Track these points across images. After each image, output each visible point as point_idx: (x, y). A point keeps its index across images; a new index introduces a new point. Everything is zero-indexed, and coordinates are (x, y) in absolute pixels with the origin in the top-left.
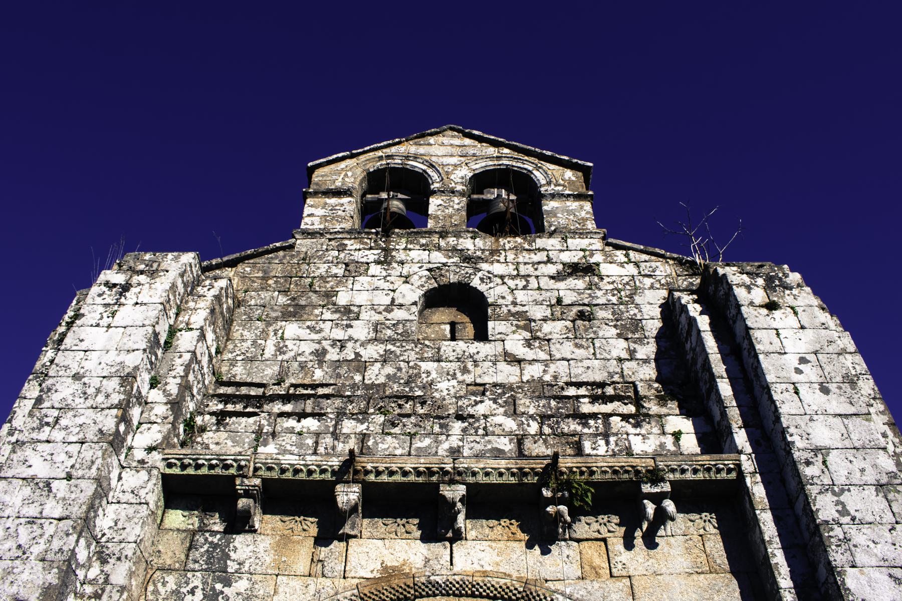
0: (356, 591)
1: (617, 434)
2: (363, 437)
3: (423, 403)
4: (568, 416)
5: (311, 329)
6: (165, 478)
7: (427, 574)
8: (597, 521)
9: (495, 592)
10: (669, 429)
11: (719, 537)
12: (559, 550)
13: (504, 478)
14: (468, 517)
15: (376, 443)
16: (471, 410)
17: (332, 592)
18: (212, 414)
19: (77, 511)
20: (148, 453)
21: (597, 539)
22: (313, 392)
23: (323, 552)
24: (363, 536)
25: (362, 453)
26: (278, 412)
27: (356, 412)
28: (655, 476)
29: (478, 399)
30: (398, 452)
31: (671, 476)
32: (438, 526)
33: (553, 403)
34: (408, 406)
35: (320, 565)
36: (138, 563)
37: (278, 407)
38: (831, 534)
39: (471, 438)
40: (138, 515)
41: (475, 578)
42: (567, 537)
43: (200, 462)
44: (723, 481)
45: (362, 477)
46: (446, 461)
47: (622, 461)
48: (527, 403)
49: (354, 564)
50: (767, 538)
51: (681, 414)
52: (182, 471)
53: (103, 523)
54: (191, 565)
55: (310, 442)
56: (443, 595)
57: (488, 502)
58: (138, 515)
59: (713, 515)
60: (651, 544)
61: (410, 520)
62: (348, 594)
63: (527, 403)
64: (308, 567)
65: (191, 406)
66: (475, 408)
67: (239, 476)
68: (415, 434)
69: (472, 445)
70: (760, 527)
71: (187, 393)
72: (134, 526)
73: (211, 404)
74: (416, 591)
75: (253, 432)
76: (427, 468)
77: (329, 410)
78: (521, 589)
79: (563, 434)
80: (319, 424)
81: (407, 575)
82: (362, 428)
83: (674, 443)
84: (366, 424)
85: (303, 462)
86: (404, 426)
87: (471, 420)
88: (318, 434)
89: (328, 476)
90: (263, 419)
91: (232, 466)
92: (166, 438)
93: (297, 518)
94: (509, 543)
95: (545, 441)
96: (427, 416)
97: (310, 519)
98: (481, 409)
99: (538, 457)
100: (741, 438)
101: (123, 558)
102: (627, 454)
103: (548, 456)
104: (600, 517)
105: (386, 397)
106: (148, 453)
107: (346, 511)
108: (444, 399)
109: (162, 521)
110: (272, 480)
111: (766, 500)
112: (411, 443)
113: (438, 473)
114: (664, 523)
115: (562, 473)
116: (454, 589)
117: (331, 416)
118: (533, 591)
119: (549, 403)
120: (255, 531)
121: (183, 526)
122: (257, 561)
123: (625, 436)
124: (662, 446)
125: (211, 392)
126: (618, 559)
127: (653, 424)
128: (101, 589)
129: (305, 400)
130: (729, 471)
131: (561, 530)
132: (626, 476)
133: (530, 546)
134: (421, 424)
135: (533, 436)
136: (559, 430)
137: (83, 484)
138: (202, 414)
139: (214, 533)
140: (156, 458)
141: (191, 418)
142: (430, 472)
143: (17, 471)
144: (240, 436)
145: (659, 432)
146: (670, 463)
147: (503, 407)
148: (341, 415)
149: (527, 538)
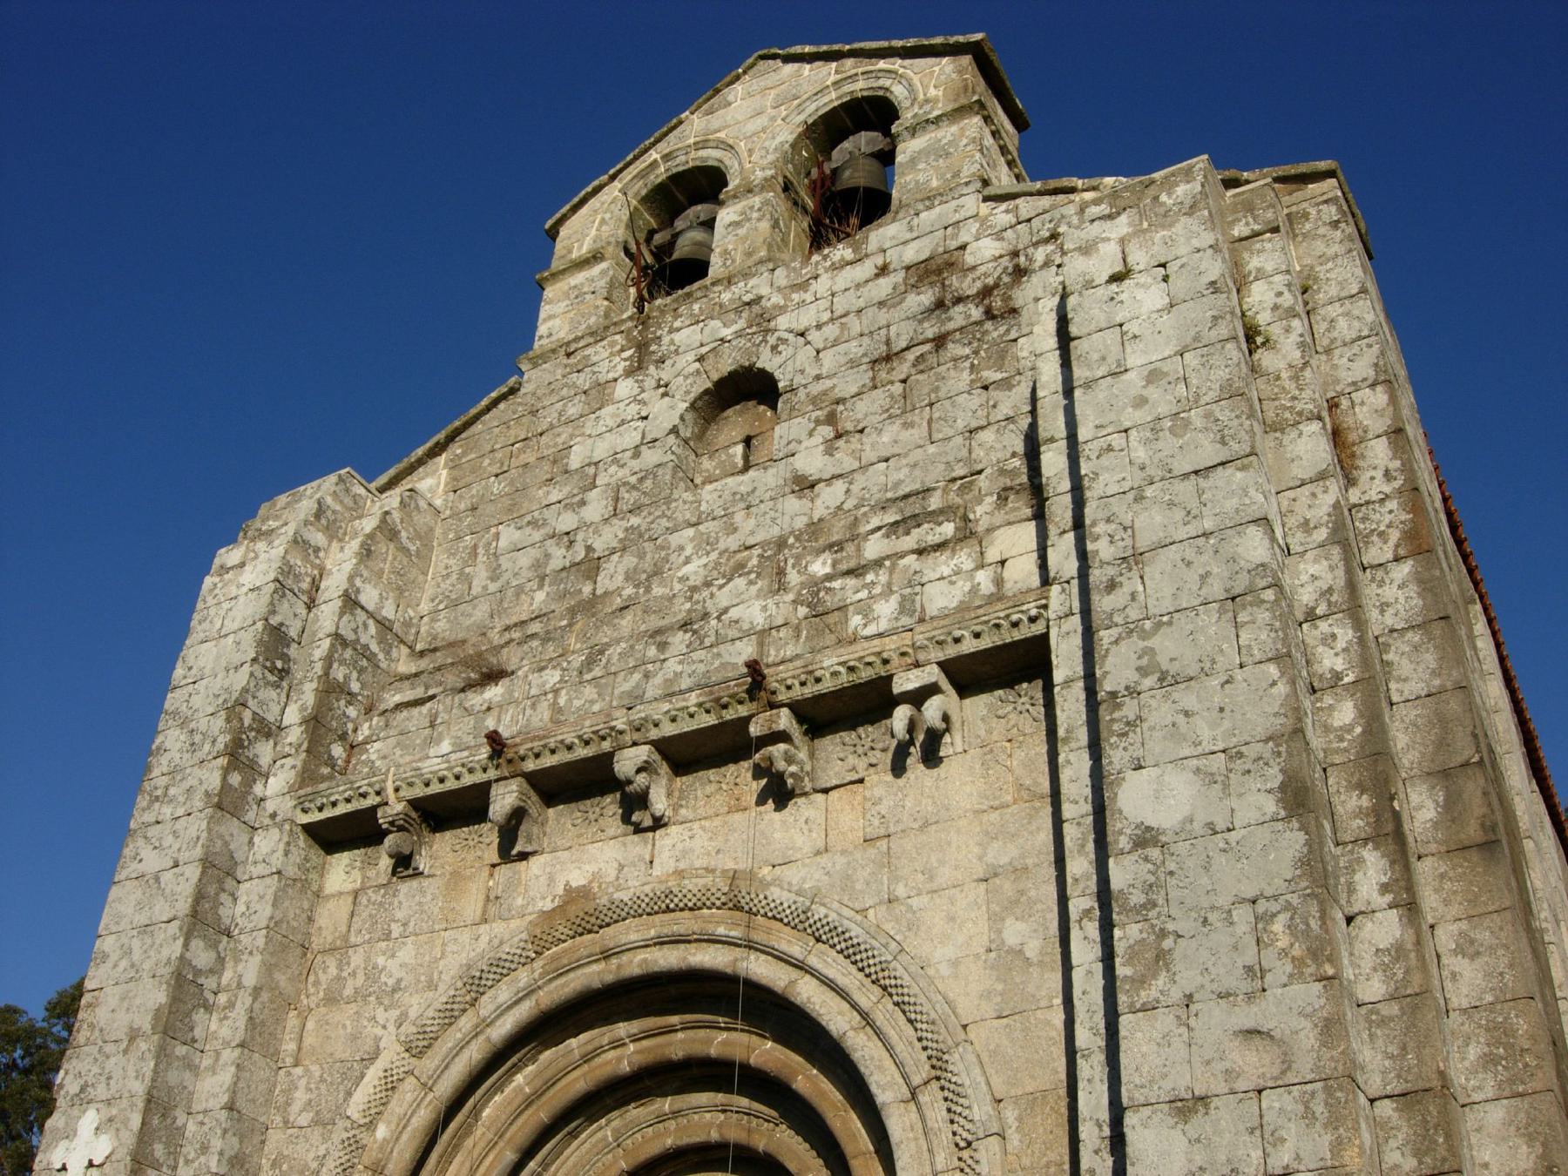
5: (533, 524)
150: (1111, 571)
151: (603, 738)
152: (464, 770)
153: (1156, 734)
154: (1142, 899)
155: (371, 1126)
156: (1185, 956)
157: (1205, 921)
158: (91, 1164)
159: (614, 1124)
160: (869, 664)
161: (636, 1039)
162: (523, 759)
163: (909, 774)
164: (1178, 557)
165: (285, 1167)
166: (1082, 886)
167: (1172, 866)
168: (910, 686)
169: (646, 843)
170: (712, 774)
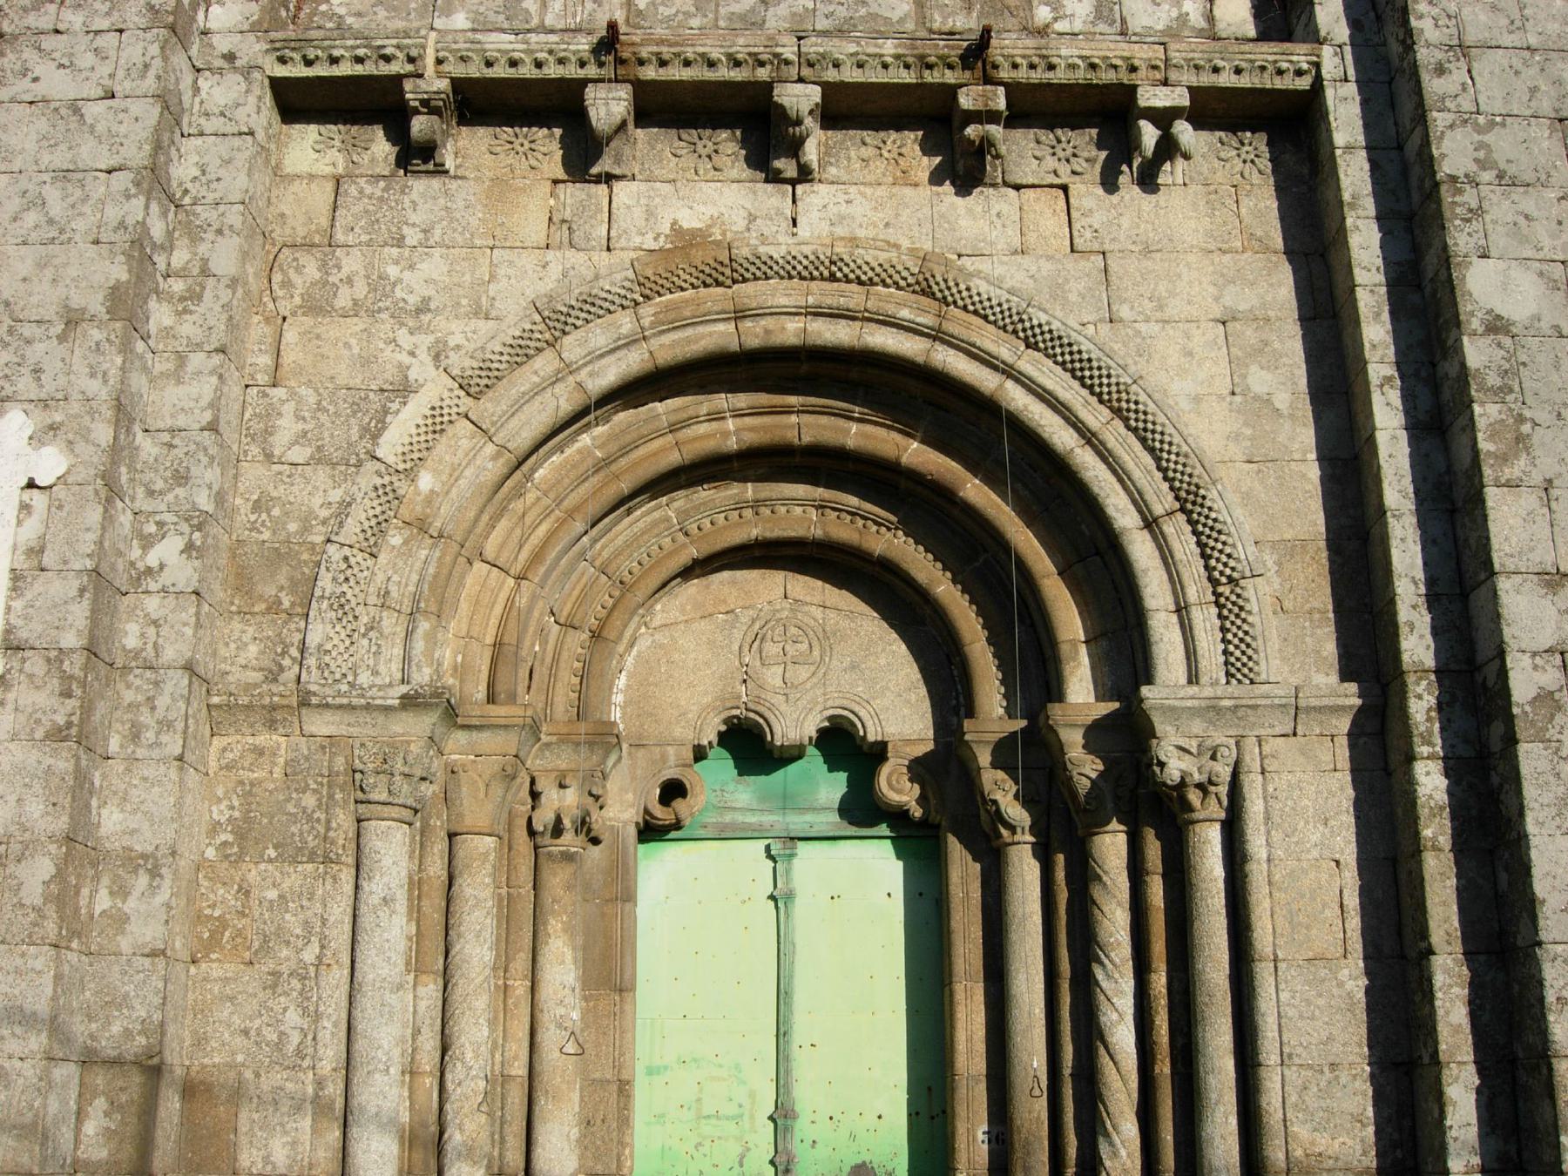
6: (277, 85)
17: (590, 275)
19: (136, 153)
21: (1051, 186)
35: (565, 227)
38: (1457, 199)
50: (1346, 197)
53: (182, 171)
62: (618, 277)
64: (545, 233)
78: (916, 270)
81: (717, 243)
94: (895, 190)
114: (1171, 158)
128: (200, 284)
130: (1299, 73)
137: (136, 107)
143: (15, 89)
150: (1439, 55)
151: (762, 64)
152: (551, 59)
153: (1500, 229)
154: (1498, 382)
155: (410, 474)
156: (1543, 444)
157: (1559, 414)
158: (31, 485)
159: (676, 505)
160: (1115, 67)
161: (738, 414)
162: (641, 62)
163: (1122, 192)
164: (1505, 63)
165: (276, 512)
166: (1380, 352)
167: (1523, 358)
168: (1159, 103)
169: (784, 195)
170: (869, 136)
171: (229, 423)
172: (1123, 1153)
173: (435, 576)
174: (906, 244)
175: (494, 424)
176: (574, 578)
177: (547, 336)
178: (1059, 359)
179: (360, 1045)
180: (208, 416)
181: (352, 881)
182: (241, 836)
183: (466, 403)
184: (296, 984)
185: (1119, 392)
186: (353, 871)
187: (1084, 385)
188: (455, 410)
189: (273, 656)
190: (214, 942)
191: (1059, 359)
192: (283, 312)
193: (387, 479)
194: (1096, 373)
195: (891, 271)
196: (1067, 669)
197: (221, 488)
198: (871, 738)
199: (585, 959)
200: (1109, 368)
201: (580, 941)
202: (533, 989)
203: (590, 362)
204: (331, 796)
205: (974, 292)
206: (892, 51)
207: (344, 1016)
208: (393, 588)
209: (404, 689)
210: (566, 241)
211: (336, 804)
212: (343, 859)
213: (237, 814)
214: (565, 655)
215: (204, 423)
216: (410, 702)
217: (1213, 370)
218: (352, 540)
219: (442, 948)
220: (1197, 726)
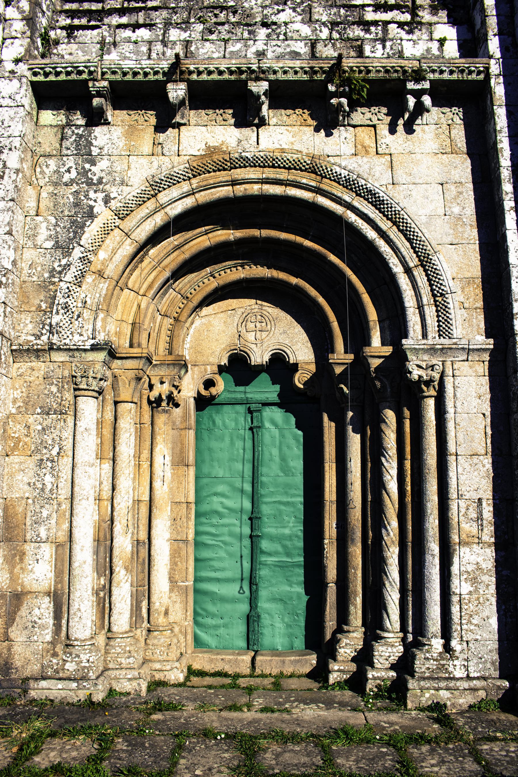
0: (187, 165)
1: (392, 40)
2: (187, 43)
3: (235, 13)
4: (354, 23)
6: (33, 83)
7: (240, 151)
8: (370, 112)
9: (290, 164)
10: (437, 35)
11: (463, 126)
12: (341, 134)
13: (299, 75)
14: (270, 107)
15: (197, 48)
16: (274, 18)
17: (170, 166)
18: (62, 28)
20: (16, 65)
21: (368, 126)
22: (143, 5)
23: (162, 137)
24: (191, 124)
25: (186, 57)
26: (116, 24)
27: (179, 21)
28: (418, 75)
29: (281, 8)
30: (216, 55)
31: (431, 76)
32: (247, 115)
33: (342, 11)
34: (222, 15)
36: (25, 151)
37: (115, 20)
39: (274, 43)
40: (18, 116)
41: (275, 154)
42: (346, 123)
43: (58, 70)
44: (473, 81)
45: (187, 76)
46: (252, 62)
47: (394, 62)
48: (321, 12)
49: (185, 145)
50: (498, 128)
51: (448, 23)
52: (46, 78)
54: (65, 152)
55: (144, 49)
56: (251, 167)
57: (287, 95)
58: (18, 116)
59: (461, 110)
60: (409, 129)
61: (226, 111)
62: (182, 167)
63: (321, 12)
64: (151, 148)
65: (44, 22)
66: (278, 16)
67: (91, 80)
68: (228, 40)
69: (275, 48)
70: (494, 120)
71: (38, 10)
72: (16, 124)
73: (60, 19)
74: (231, 164)
75: (98, 43)
76: (238, 68)
77: (158, 21)
78: (309, 162)
79: (349, 39)
80: (150, 33)
81: (224, 152)
82: (185, 35)
83: (438, 48)
84: (189, 32)
85: (140, 66)
86: (220, 33)
87: (274, 27)
88: (150, 43)
89: (160, 77)
90: (104, 31)
91: (84, 72)
92: (28, 51)
93: (139, 111)
95: (334, 45)
96: (238, 24)
97: (150, 112)
98: (282, 17)
99: (327, 58)
100: (494, 45)
101: (13, 149)
102: (399, 57)
103: (335, 57)
104: (372, 109)
105: (204, 7)
106: (16, 65)
107: (176, 105)
108: (252, 9)
109: (37, 119)
110: (116, 82)
111: (504, 98)
112: (225, 48)
113: (246, 71)
115: (345, 72)
116: (259, 162)
117: (159, 26)
118: (318, 163)
119: (339, 12)
120: (109, 123)
121: (54, 123)
122: (113, 146)
123: (399, 41)
124: (428, 50)
125: (59, 8)
126: (383, 141)
127: (424, 31)
129: (137, 13)
130: (479, 73)
131: (341, 118)
132: (395, 75)
133: (317, 130)
134: (233, 31)
135: (324, 41)
136: (346, 36)
138: (54, 29)
139: (78, 127)
140: (22, 68)
141: (45, 32)
142: (240, 71)
144: (88, 47)
145: (427, 38)
146: (432, 65)
147: (301, 15)
148: (168, 24)
149: (315, 124)
155: (95, 252)
171: (17, 231)
172: (392, 534)
173: (106, 295)
174: (305, 151)
175: (130, 230)
176: (167, 296)
177: (152, 192)
178: (370, 200)
179: (76, 489)
180: (7, 228)
181: (73, 422)
182: (26, 403)
183: (118, 222)
184: (49, 464)
185: (395, 214)
186: (73, 418)
187: (380, 212)
188: (113, 224)
189: (38, 329)
190: (16, 447)
191: (370, 200)
192: (41, 184)
193: (85, 254)
194: (386, 206)
195: (298, 163)
196: (372, 333)
197: (15, 259)
198: (291, 362)
199: (173, 453)
200: (391, 204)
201: (170, 445)
202: (151, 466)
203: (171, 204)
204: (63, 387)
205: (334, 171)
206: (299, 66)
207: (70, 477)
208: (88, 299)
209: (92, 342)
210: (160, 152)
211: (65, 390)
212: (68, 412)
213: (24, 395)
214: (163, 328)
215: (6, 231)
216: (95, 348)
217: (437, 205)
218: (71, 280)
219: (112, 448)
220: (426, 357)
